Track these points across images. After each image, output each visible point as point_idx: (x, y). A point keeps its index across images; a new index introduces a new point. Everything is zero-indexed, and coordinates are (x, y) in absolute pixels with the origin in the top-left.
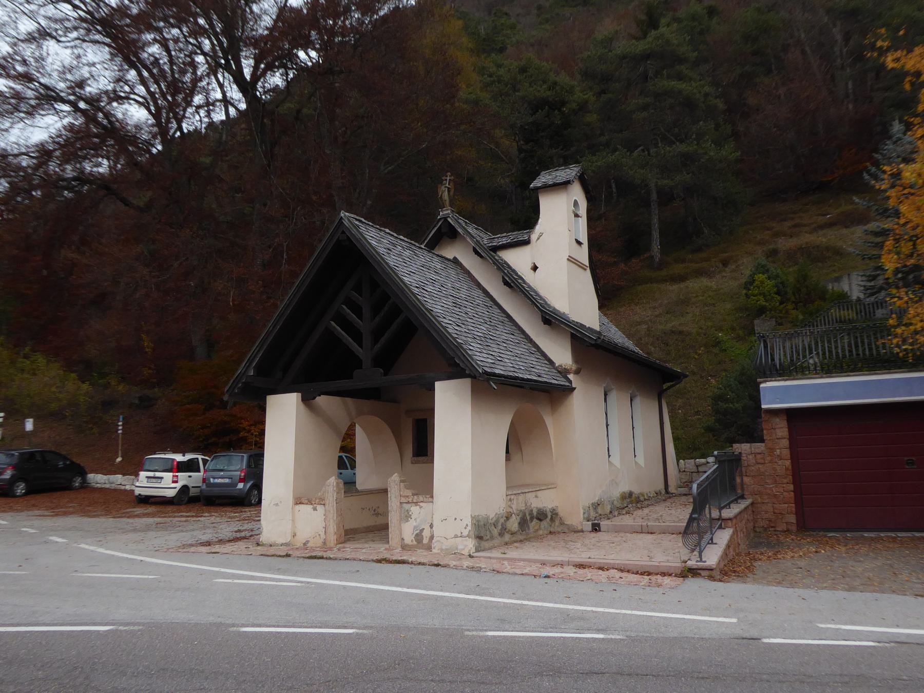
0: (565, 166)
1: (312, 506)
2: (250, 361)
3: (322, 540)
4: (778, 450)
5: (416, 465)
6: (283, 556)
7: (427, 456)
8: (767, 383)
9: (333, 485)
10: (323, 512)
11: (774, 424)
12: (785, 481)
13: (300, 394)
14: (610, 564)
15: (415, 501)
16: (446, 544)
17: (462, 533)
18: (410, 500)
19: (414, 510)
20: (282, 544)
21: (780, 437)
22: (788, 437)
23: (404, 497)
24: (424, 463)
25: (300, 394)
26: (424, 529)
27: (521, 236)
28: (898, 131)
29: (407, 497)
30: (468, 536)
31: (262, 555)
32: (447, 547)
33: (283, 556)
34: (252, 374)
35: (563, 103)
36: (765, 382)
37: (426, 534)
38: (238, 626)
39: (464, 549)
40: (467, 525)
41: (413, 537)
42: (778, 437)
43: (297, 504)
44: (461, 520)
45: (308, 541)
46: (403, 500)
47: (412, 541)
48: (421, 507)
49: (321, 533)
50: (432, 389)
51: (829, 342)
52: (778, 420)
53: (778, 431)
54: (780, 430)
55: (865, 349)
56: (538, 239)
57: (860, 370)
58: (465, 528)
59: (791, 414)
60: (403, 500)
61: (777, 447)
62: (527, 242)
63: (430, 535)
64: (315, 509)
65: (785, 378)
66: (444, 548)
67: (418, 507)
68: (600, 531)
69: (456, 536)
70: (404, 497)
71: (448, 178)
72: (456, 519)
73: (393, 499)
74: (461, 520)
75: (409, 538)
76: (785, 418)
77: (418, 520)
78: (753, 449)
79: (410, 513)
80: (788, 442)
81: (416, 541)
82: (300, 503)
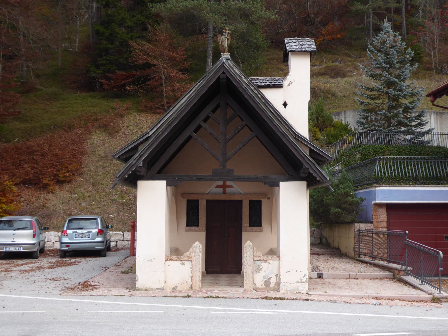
1: (180, 262)
2: (141, 156)
6: (186, 297)
7: (198, 226)
9: (200, 248)
13: (138, 181)
14: (393, 296)
15: (265, 259)
16: (290, 287)
17: (301, 280)
18: (261, 258)
19: (264, 265)
23: (257, 256)
24: (195, 231)
25: (138, 181)
28: (388, 26)
29: (259, 256)
30: (305, 282)
31: (165, 296)
33: (186, 297)
34: (142, 165)
36: (379, 186)
37: (273, 281)
40: (305, 275)
41: (262, 283)
42: (381, 220)
43: (167, 260)
44: (301, 272)
45: (176, 287)
46: (256, 258)
47: (262, 285)
48: (269, 263)
49: (188, 281)
50: (278, 186)
51: (411, 165)
53: (381, 216)
54: (383, 215)
55: (443, 173)
56: (289, 85)
57: (425, 183)
58: (304, 277)
59: (390, 208)
60: (256, 258)
62: (281, 86)
64: (183, 264)
65: (390, 185)
66: (289, 289)
67: (267, 263)
68: (323, 278)
69: (297, 282)
70: (257, 256)
71: (227, 32)
72: (297, 271)
73: (248, 258)
74: (301, 272)
75: (260, 283)
76: (386, 209)
77: (267, 272)
78: (366, 227)
79: (261, 267)
82: (170, 260)
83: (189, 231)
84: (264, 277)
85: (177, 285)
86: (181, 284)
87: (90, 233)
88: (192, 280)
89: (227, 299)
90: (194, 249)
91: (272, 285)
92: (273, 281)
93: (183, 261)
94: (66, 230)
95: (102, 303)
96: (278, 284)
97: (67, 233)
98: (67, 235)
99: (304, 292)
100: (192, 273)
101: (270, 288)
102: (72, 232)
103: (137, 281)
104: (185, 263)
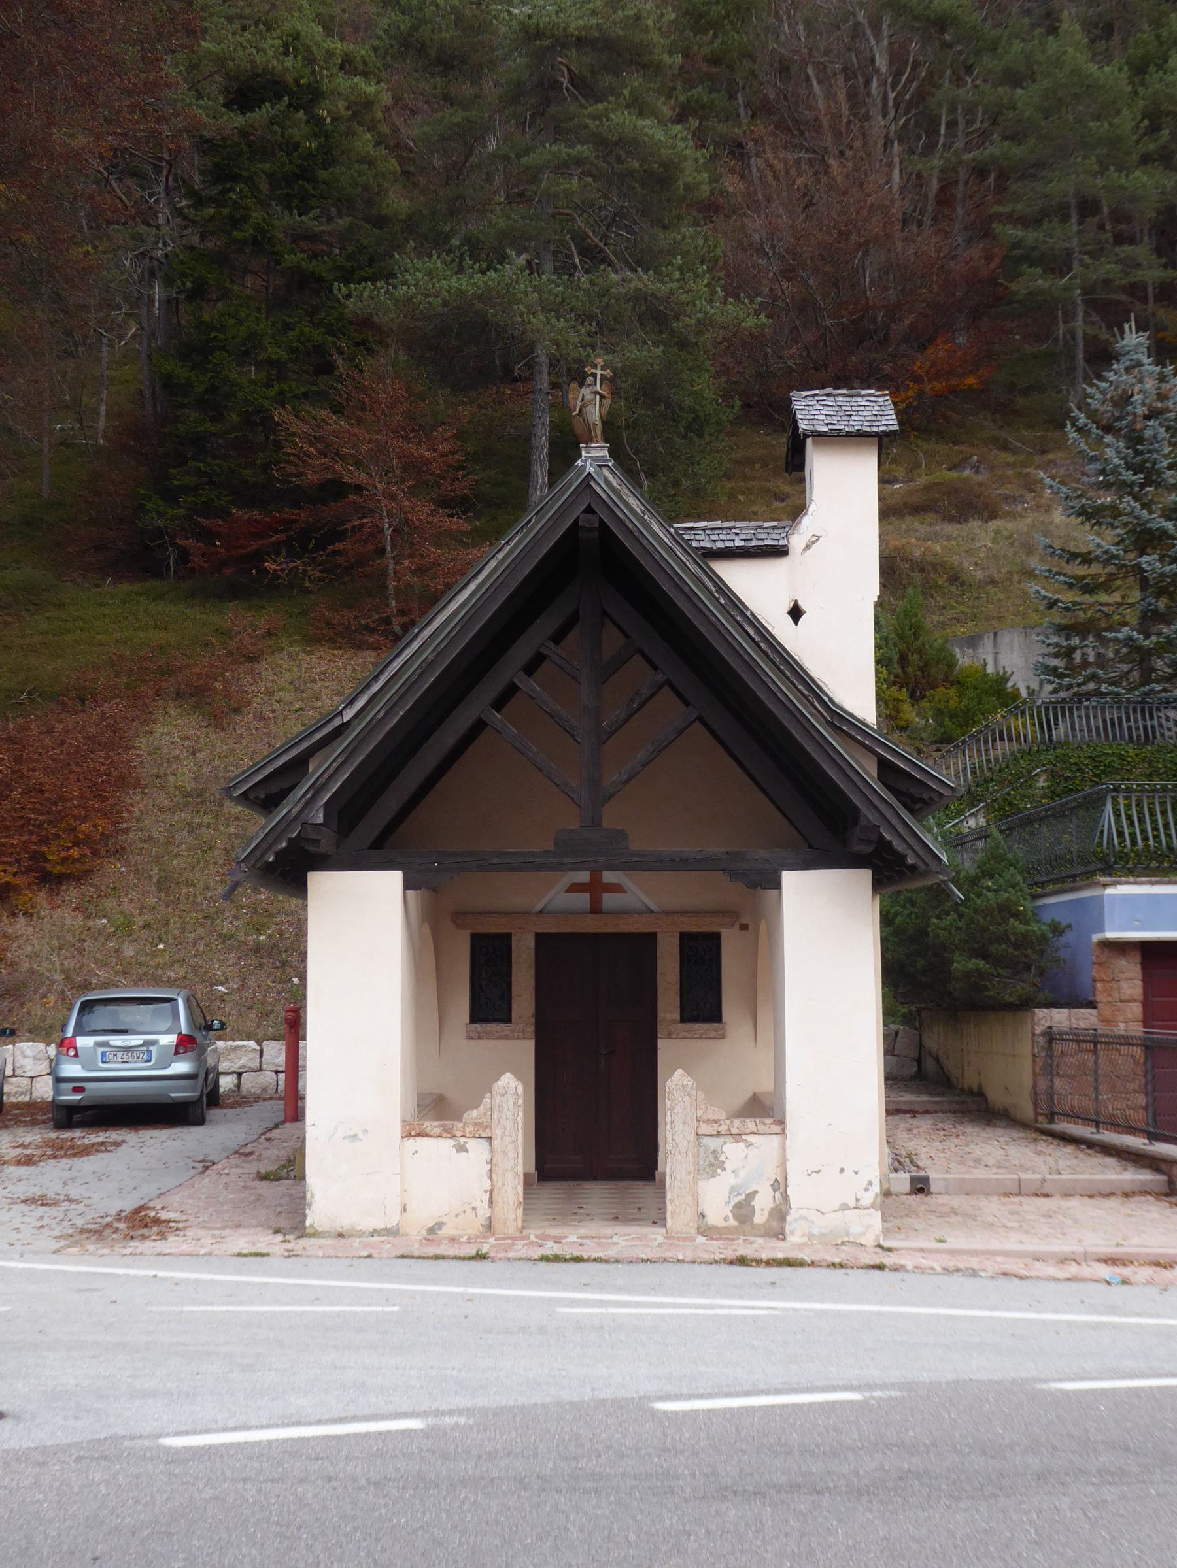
0: (878, 389)
1: (452, 1142)
2: (317, 790)
3: (482, 1220)
4: (1122, 1025)
5: (482, 1042)
8: (1119, 887)
10: (486, 1156)
11: (1117, 971)
12: (1131, 1087)
15: (734, 1131)
17: (857, 1200)
18: (723, 1129)
19: (732, 1151)
20: (375, 1231)
21: (1127, 997)
22: (1141, 998)
23: (707, 1121)
26: (756, 1192)
27: (762, 532)
29: (716, 1122)
30: (873, 1206)
32: (823, 1231)
34: (320, 820)
35: (315, 94)
37: (764, 1204)
38: (1046, 1381)
39: (864, 1234)
40: (870, 1183)
41: (727, 1211)
42: (1123, 998)
43: (409, 1136)
44: (856, 1173)
45: (440, 1225)
46: (705, 1129)
47: (726, 1219)
49: (478, 1204)
52: (1124, 962)
56: (808, 547)
58: (866, 1189)
60: (705, 1129)
61: (1121, 1018)
62: (780, 552)
63: (772, 1205)
64: (462, 1149)
65: (1153, 879)
66: (816, 1231)
67: (741, 1145)
69: (844, 1207)
72: (842, 1170)
73: (679, 1126)
74: (856, 1173)
76: (1138, 958)
77: (742, 1174)
79: (722, 1158)
80: (1141, 1009)
81: (736, 1217)
82: (419, 1135)
83: (480, 1038)
84: (733, 1190)
85: (444, 1219)
86: (457, 1216)
87: (151, 1048)
88: (491, 1202)
89: (611, 1267)
90: (498, 1099)
91: (760, 1218)
92: (764, 1204)
93: (462, 1140)
94: (74, 1036)
95: (197, 1281)
96: (780, 1213)
97: (75, 1048)
98: (76, 1055)
99: (869, 1240)
100: (491, 1178)
101: (753, 1226)
102: (91, 1045)
103: (310, 1205)
104: (468, 1146)
